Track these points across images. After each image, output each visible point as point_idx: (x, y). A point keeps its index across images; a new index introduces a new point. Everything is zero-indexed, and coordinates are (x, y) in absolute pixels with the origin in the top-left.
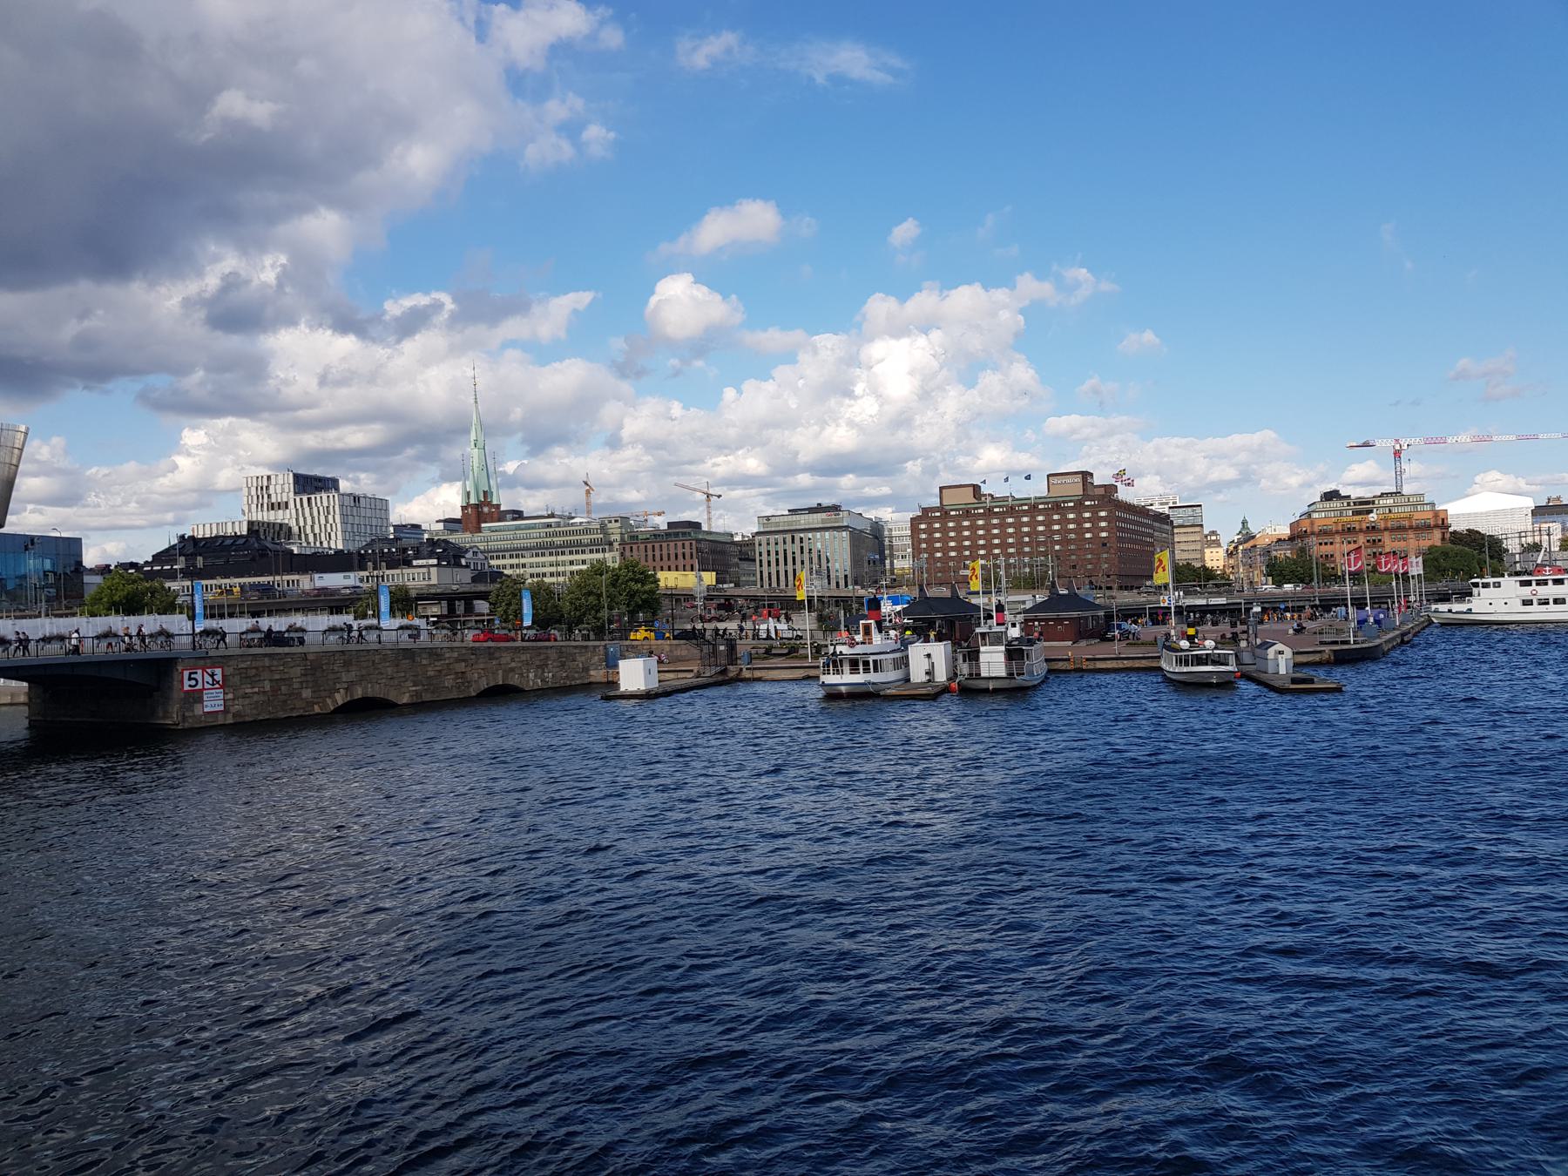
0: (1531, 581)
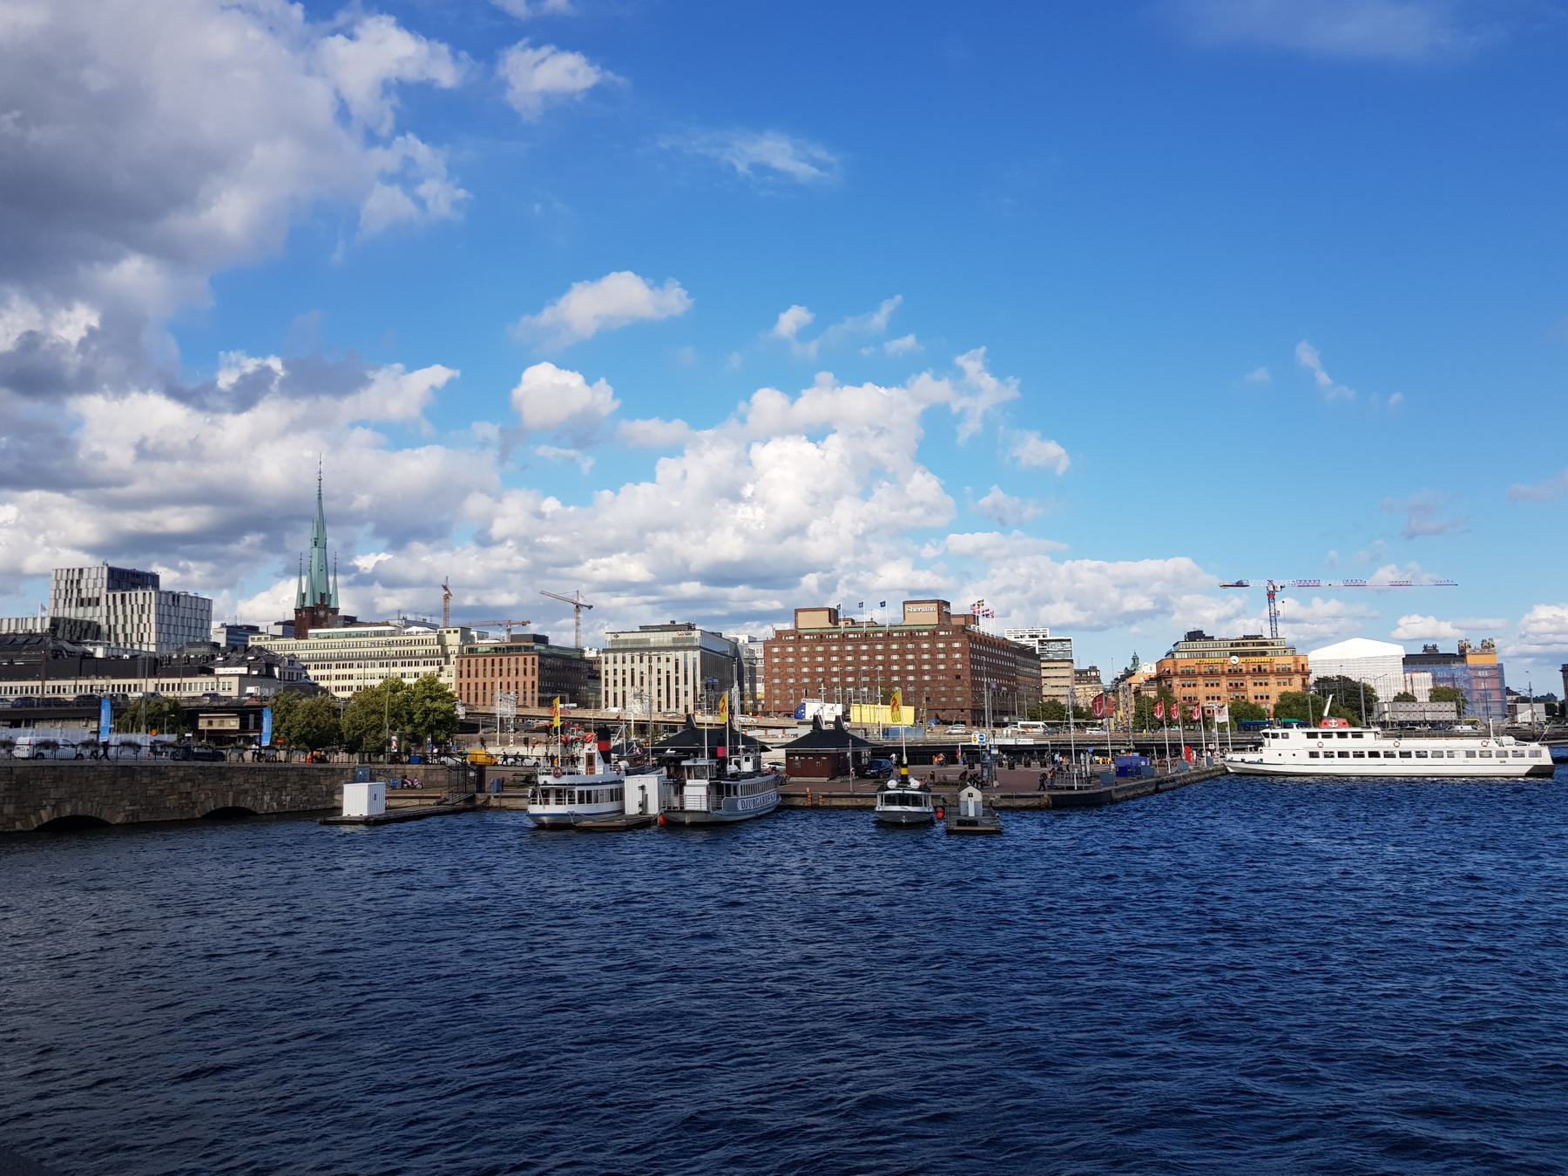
0: (1317, 733)
